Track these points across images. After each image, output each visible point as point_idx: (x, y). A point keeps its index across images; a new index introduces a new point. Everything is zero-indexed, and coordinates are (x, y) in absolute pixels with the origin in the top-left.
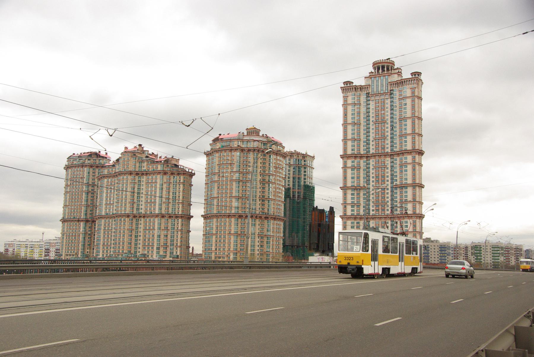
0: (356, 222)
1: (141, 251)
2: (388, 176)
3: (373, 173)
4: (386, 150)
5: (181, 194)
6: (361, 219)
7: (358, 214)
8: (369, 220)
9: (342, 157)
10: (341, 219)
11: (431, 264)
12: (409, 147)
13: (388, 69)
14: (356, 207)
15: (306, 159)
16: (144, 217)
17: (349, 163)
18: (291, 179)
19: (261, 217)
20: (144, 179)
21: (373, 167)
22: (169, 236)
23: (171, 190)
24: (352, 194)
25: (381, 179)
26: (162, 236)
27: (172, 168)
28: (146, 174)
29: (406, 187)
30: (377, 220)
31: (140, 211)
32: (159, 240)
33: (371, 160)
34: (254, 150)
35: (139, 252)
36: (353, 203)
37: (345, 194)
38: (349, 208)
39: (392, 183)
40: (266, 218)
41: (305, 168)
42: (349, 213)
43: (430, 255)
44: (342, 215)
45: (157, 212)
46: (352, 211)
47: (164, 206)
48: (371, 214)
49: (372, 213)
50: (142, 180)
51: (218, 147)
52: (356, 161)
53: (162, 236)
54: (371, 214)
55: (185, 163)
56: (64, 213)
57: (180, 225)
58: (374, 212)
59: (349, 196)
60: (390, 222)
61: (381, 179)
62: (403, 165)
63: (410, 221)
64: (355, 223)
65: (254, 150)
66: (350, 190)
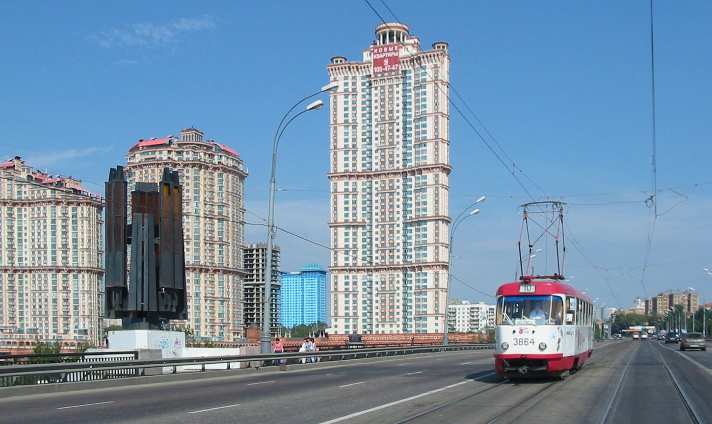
0: (351, 275)
1: (29, 323)
2: (398, 118)
4: (396, 261)
5: (85, 235)
6: (358, 176)
7: (354, 171)
11: (459, 333)
12: (430, 161)
13: (398, 39)
14: (350, 128)
16: (30, 271)
20: (27, 211)
21: (376, 148)
22: (71, 301)
25: (387, 208)
26: (60, 302)
28: (30, 204)
29: (425, 222)
31: (24, 262)
32: (55, 307)
34: (195, 269)
35: (27, 325)
39: (405, 217)
43: (457, 317)
45: (50, 263)
47: (60, 255)
48: (374, 170)
49: (374, 167)
50: (24, 213)
51: (137, 161)
52: (351, 182)
53: (60, 302)
54: (374, 170)
60: (401, 274)
61: (387, 208)
62: (421, 189)
63: (430, 273)
64: (351, 278)
65: (195, 269)
66: (343, 229)
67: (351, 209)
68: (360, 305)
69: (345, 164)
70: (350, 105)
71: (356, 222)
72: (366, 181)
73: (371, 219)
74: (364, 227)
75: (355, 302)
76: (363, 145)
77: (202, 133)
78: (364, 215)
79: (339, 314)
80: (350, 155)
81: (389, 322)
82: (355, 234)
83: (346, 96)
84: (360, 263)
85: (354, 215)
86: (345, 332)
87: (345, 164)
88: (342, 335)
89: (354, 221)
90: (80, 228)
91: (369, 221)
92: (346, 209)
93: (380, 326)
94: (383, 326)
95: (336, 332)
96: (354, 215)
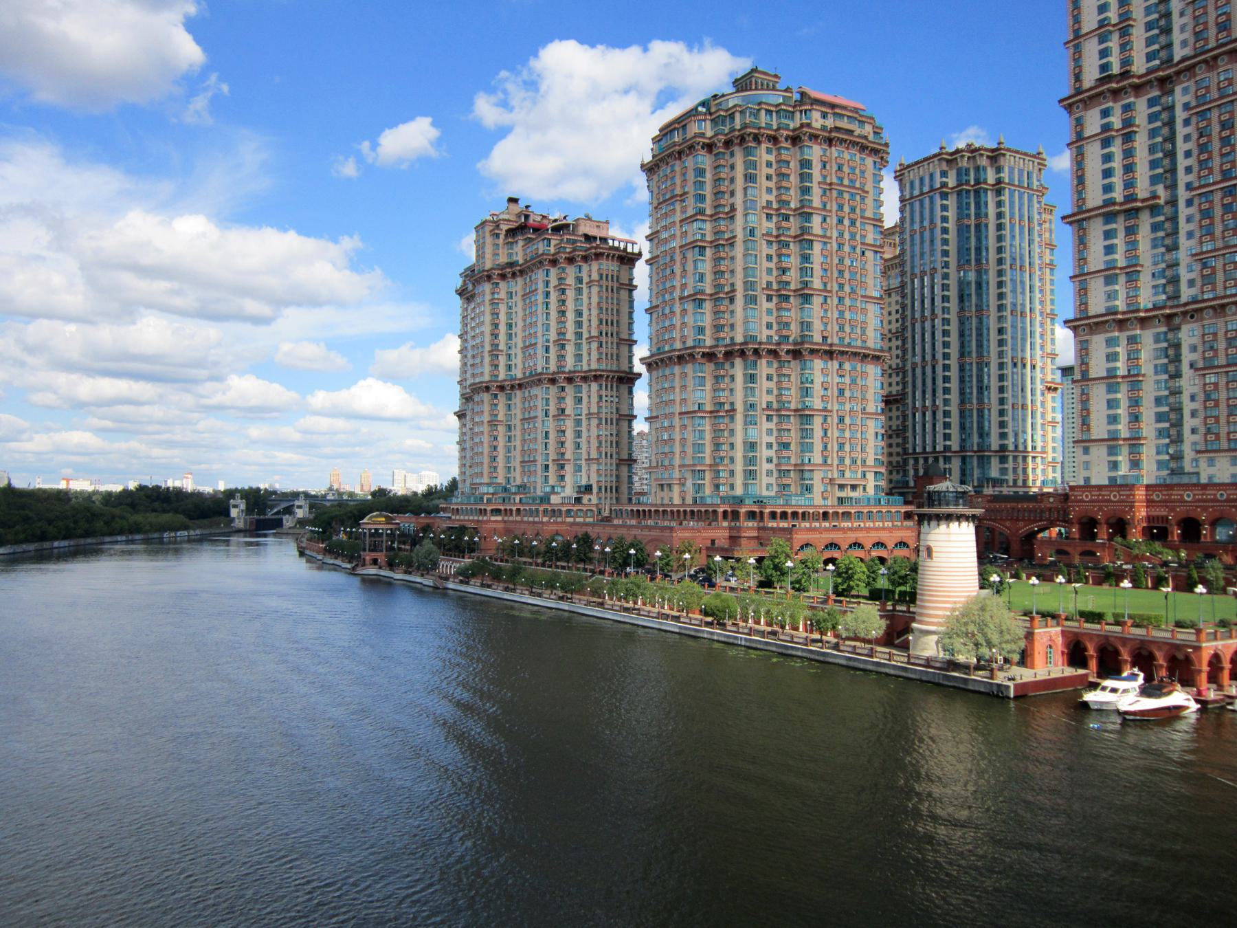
3: (1193, 398)
8: (1177, 320)
9: (1069, 105)
10: (1070, 333)
15: (1002, 161)
17: (1093, 122)
18: (952, 236)
19: (774, 353)
23: (570, 306)
24: (1108, 235)
27: (595, 248)
30: (1209, 319)
33: (1185, 328)
36: (1110, 266)
37: (1082, 242)
38: (1097, 288)
40: (796, 354)
41: (999, 192)
42: (1097, 305)
44: (1071, 316)
46: (1111, 296)
49: (1186, 293)
54: (1184, 298)
55: (616, 234)
56: (630, 392)
57: (595, 399)
58: (1193, 291)
59: (1096, 244)
67: (1119, 172)
68: (1148, 412)
69: (1109, 416)
70: (1117, 164)
71: (1136, 200)
72: (1164, 329)
73: (1172, 186)
74: (1154, 210)
75: (1135, 402)
76: (1154, 256)
77: (776, 76)
78: (1154, 180)
79: (1093, 374)
80: (1116, 149)
81: (1229, 450)
82: (1131, 231)
83: (1106, 143)
84: (1139, 66)
85: (1129, 184)
86: (1110, 478)
87: (1109, 416)
88: (1100, 487)
89: (1130, 198)
90: (585, 297)
91: (1169, 192)
92: (1107, 173)
93: (1203, 464)
94: (1211, 462)
95: (1087, 479)
96: (1129, 184)
